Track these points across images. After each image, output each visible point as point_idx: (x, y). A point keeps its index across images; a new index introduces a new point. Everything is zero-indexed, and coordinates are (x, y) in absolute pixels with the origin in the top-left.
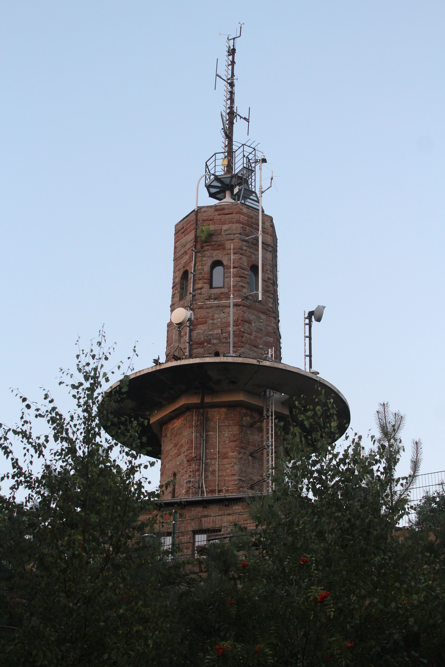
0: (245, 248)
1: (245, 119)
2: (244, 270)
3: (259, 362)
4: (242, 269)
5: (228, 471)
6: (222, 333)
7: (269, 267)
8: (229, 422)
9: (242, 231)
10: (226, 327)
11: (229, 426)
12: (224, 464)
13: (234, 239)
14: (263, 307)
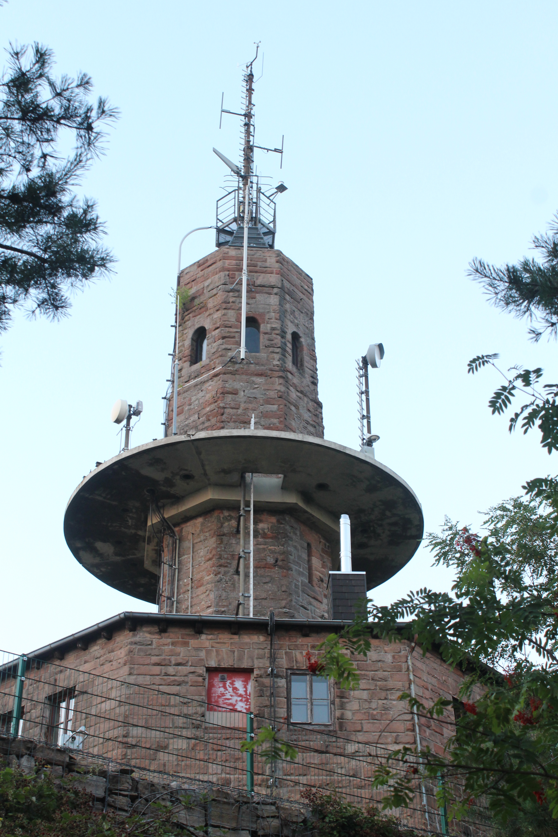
0: (231, 300)
1: (276, 150)
2: (230, 327)
3: (189, 435)
4: (226, 327)
5: (203, 603)
6: (199, 418)
7: (273, 314)
8: (205, 534)
9: (228, 280)
10: (203, 409)
11: (205, 540)
12: (198, 596)
13: (217, 294)
14: (263, 367)
